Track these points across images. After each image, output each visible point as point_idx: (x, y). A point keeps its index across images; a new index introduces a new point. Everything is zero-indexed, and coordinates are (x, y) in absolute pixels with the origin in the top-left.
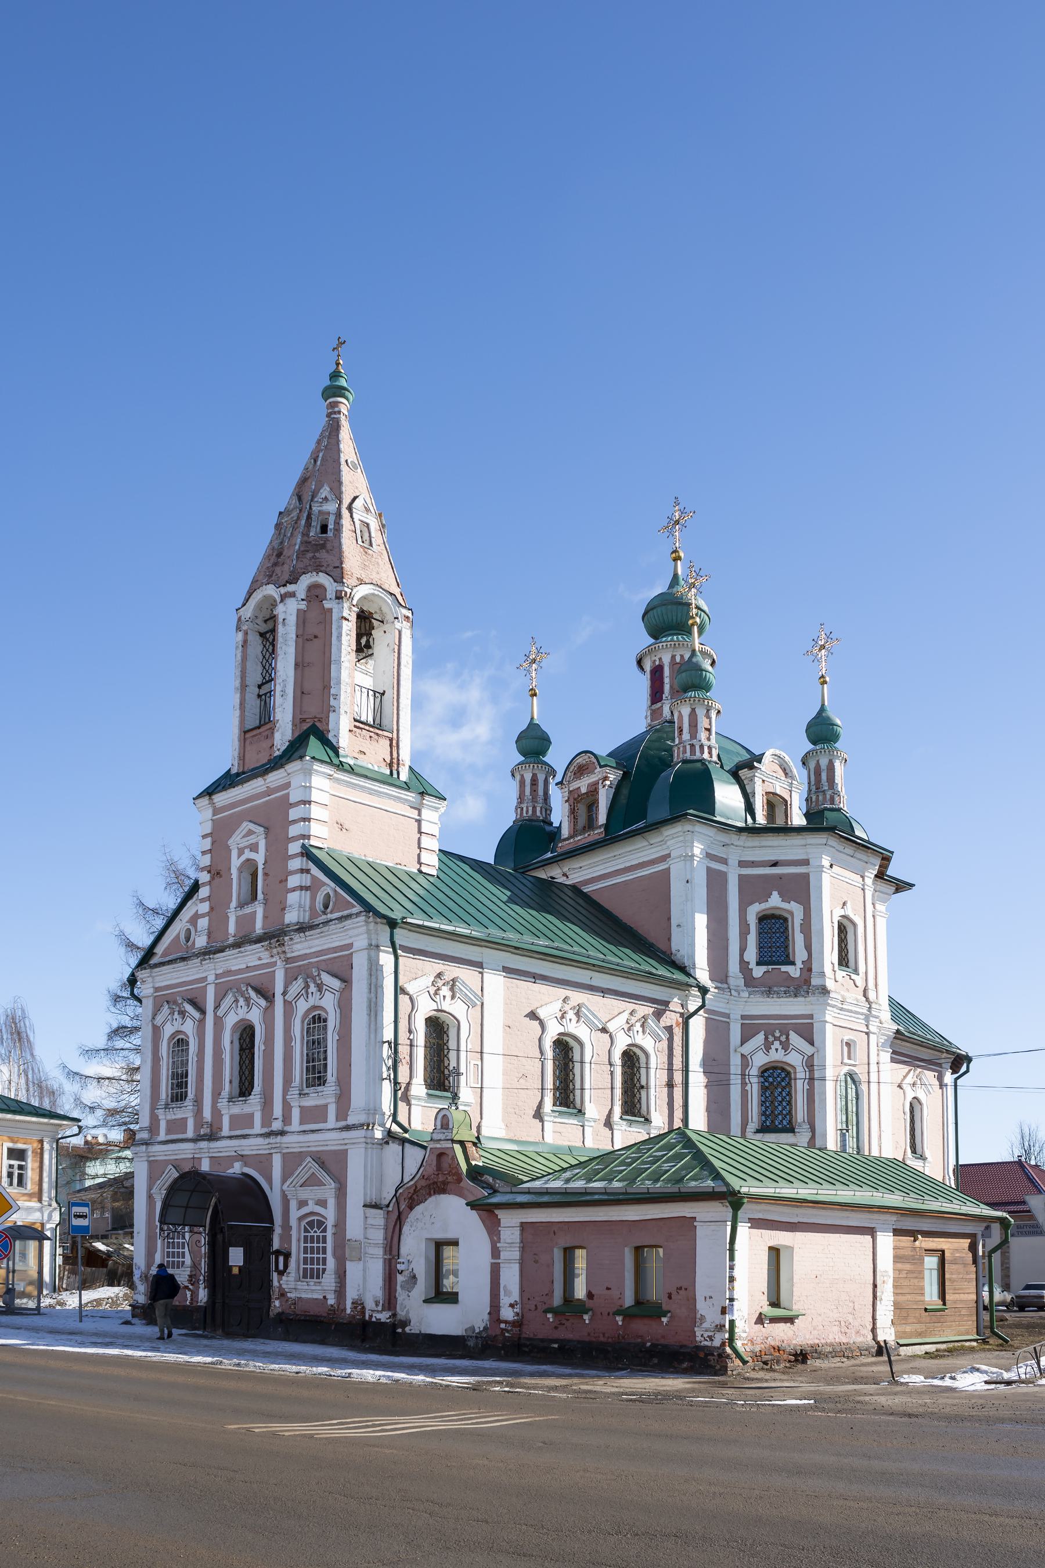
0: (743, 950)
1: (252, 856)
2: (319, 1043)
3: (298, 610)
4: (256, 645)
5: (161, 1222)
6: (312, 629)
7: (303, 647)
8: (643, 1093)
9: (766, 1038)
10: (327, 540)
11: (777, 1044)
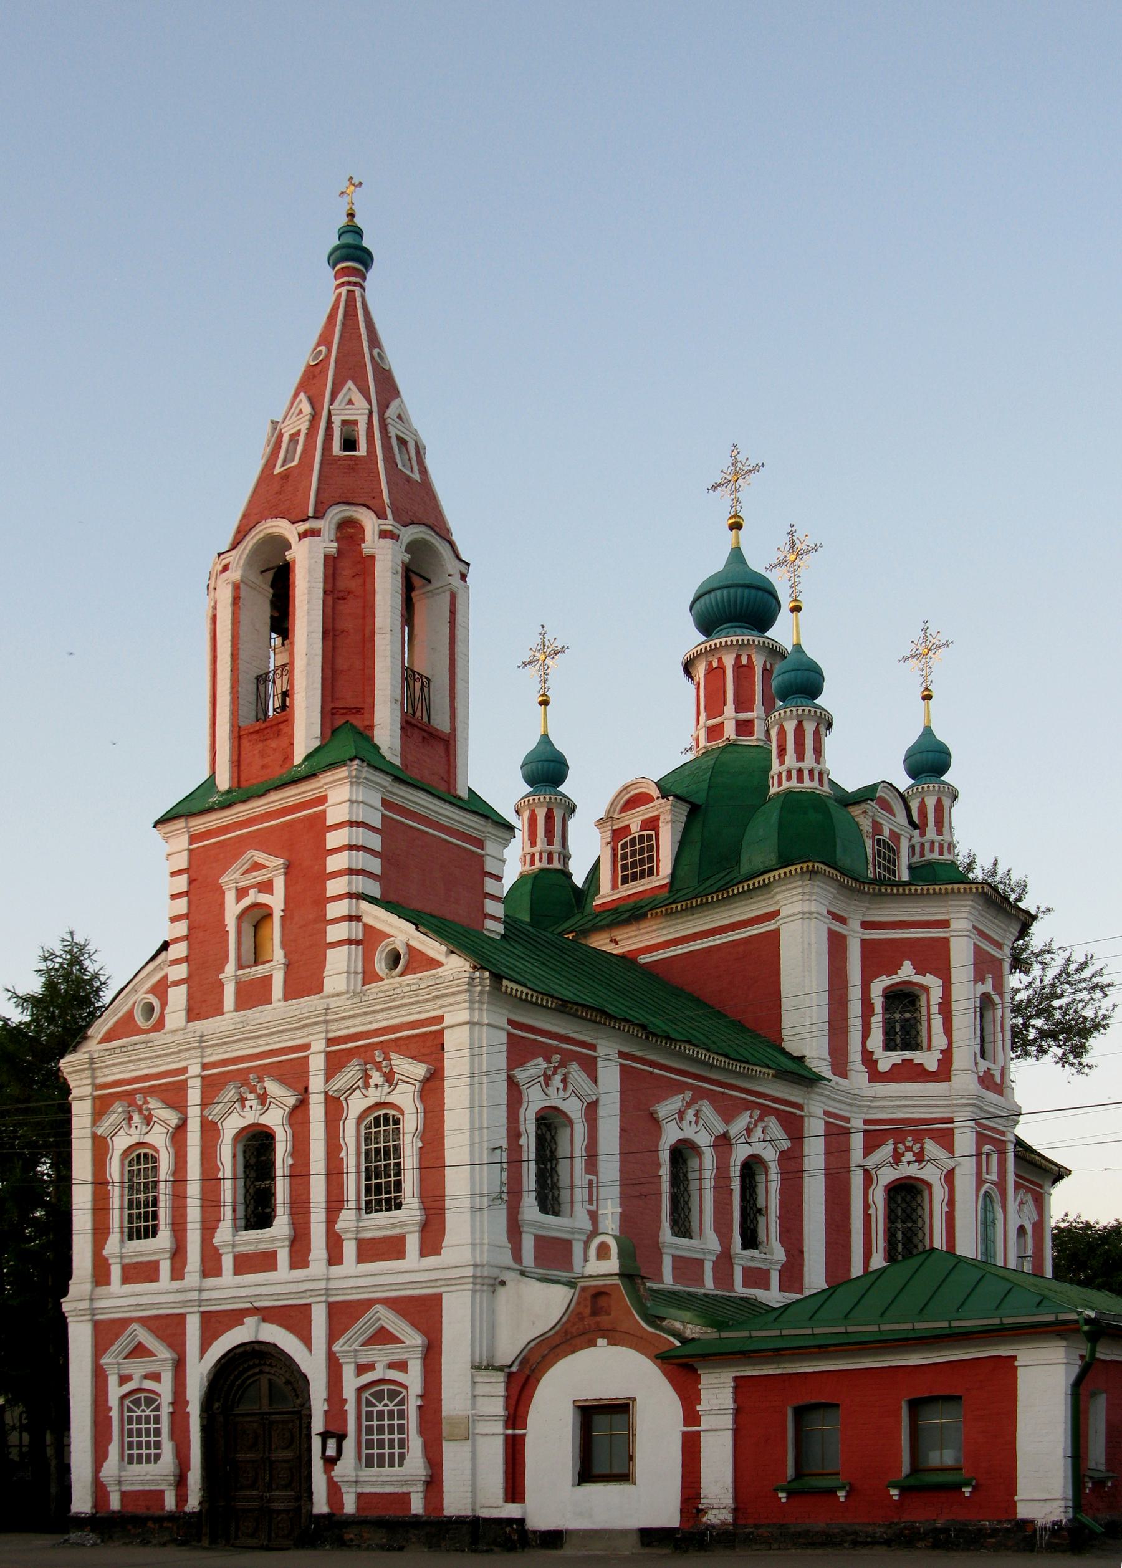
1: (263, 898)
3: (326, 556)
5: (651, 1324)
7: (334, 608)
8: (762, 1220)
9: (895, 1149)
11: (909, 1157)
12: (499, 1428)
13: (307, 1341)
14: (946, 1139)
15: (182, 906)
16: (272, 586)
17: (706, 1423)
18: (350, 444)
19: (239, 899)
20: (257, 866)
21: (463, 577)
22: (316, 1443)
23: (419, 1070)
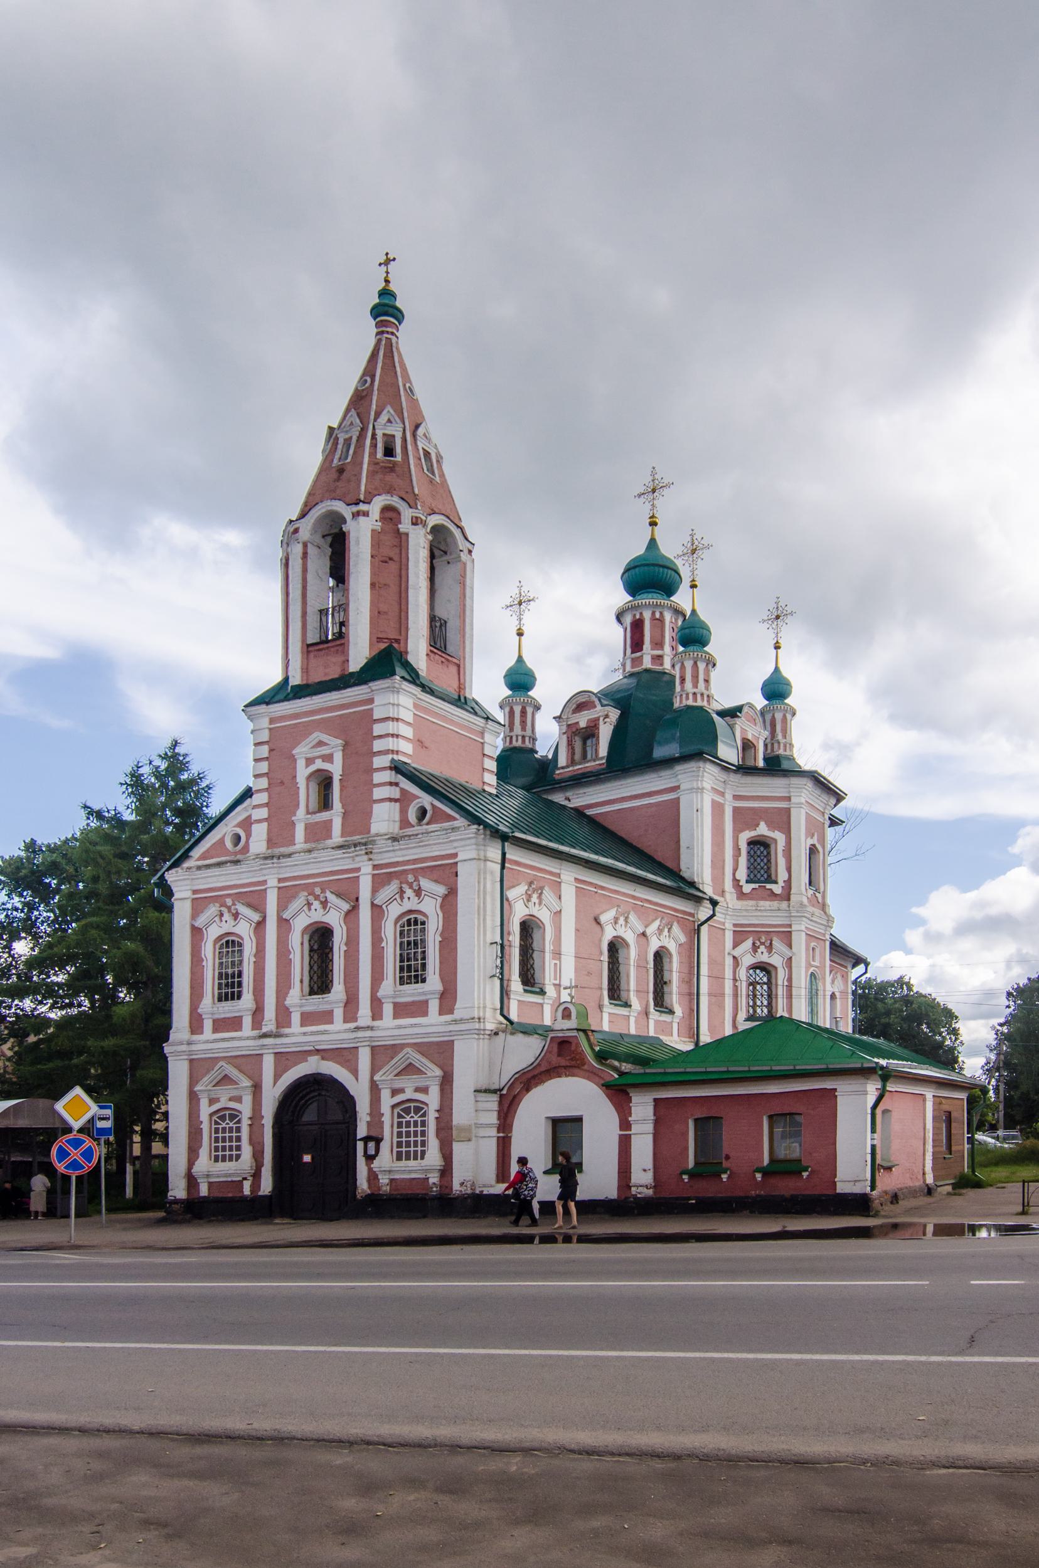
0: (735, 870)
2: (416, 944)
4: (320, 563)
6: (387, 552)
9: (754, 944)
10: (395, 464)
11: (762, 949)
12: (493, 1132)
13: (355, 1072)
14: (787, 937)
15: (264, 767)
16: (331, 546)
17: (635, 1128)
18: (389, 451)
19: (307, 766)
20: (321, 744)
21: (470, 552)
22: (360, 1146)
23: (441, 890)
